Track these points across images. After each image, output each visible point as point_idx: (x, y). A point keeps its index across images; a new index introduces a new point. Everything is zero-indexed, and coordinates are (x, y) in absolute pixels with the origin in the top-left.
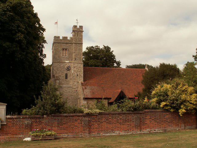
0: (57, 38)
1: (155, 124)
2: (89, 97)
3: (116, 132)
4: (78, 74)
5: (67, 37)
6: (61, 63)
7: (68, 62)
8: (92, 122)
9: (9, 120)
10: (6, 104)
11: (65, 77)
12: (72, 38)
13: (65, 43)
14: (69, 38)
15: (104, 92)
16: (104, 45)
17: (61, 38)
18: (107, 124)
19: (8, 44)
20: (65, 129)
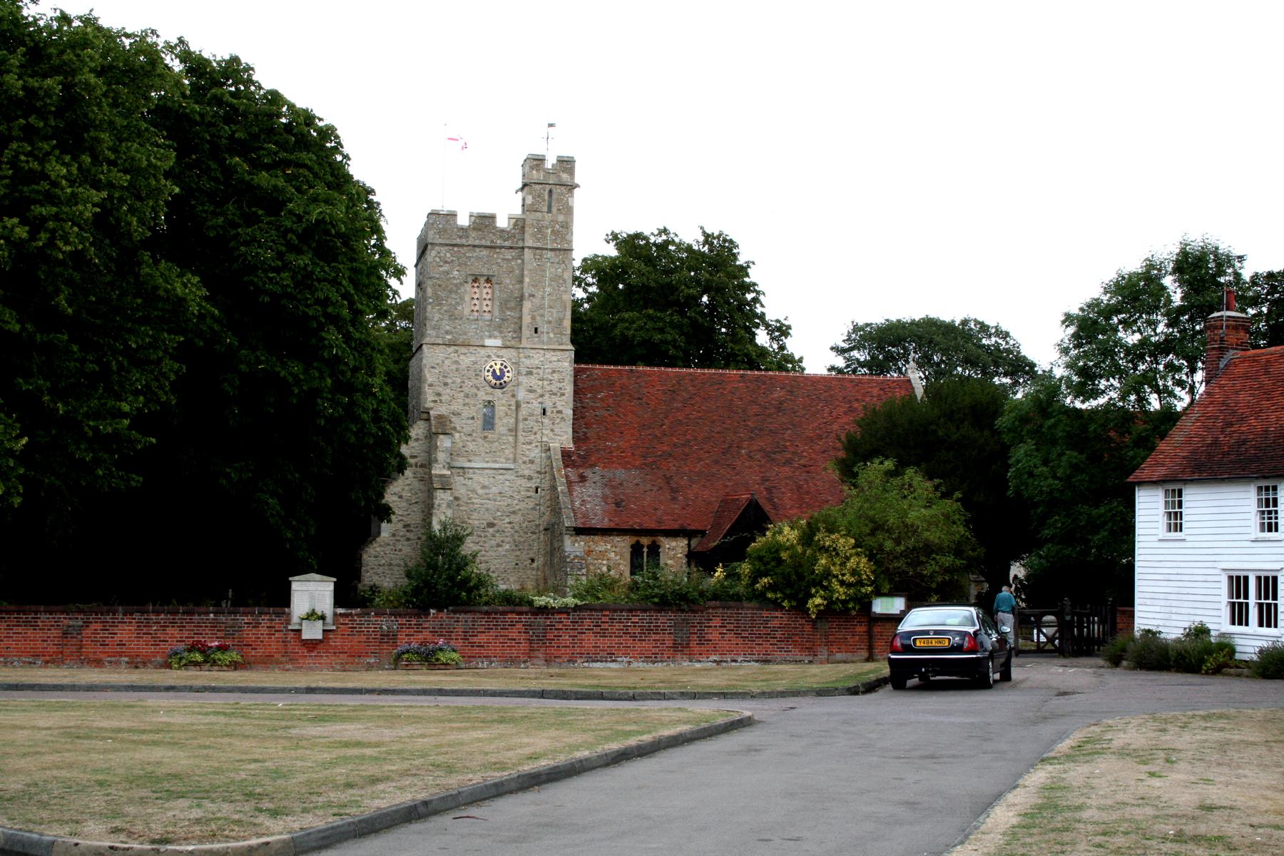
0: (439, 221)
1: (737, 644)
2: (596, 522)
3: (619, 659)
4: (548, 404)
5: (492, 217)
6: (463, 350)
7: (498, 342)
8: (556, 629)
9: (341, 620)
10: (335, 580)
11: (479, 423)
12: (518, 220)
13: (486, 247)
14: (502, 223)
15: (673, 499)
16: (702, 228)
17: (463, 221)
18: (596, 636)
19: (296, 368)
20: (483, 646)
